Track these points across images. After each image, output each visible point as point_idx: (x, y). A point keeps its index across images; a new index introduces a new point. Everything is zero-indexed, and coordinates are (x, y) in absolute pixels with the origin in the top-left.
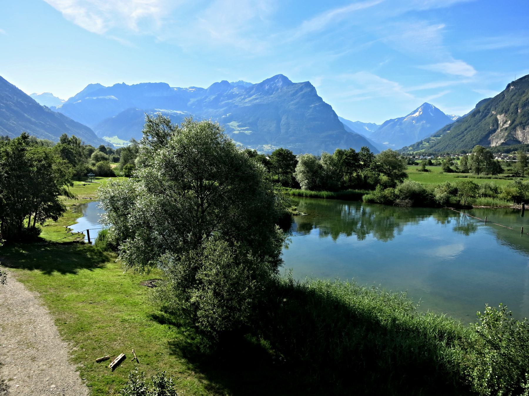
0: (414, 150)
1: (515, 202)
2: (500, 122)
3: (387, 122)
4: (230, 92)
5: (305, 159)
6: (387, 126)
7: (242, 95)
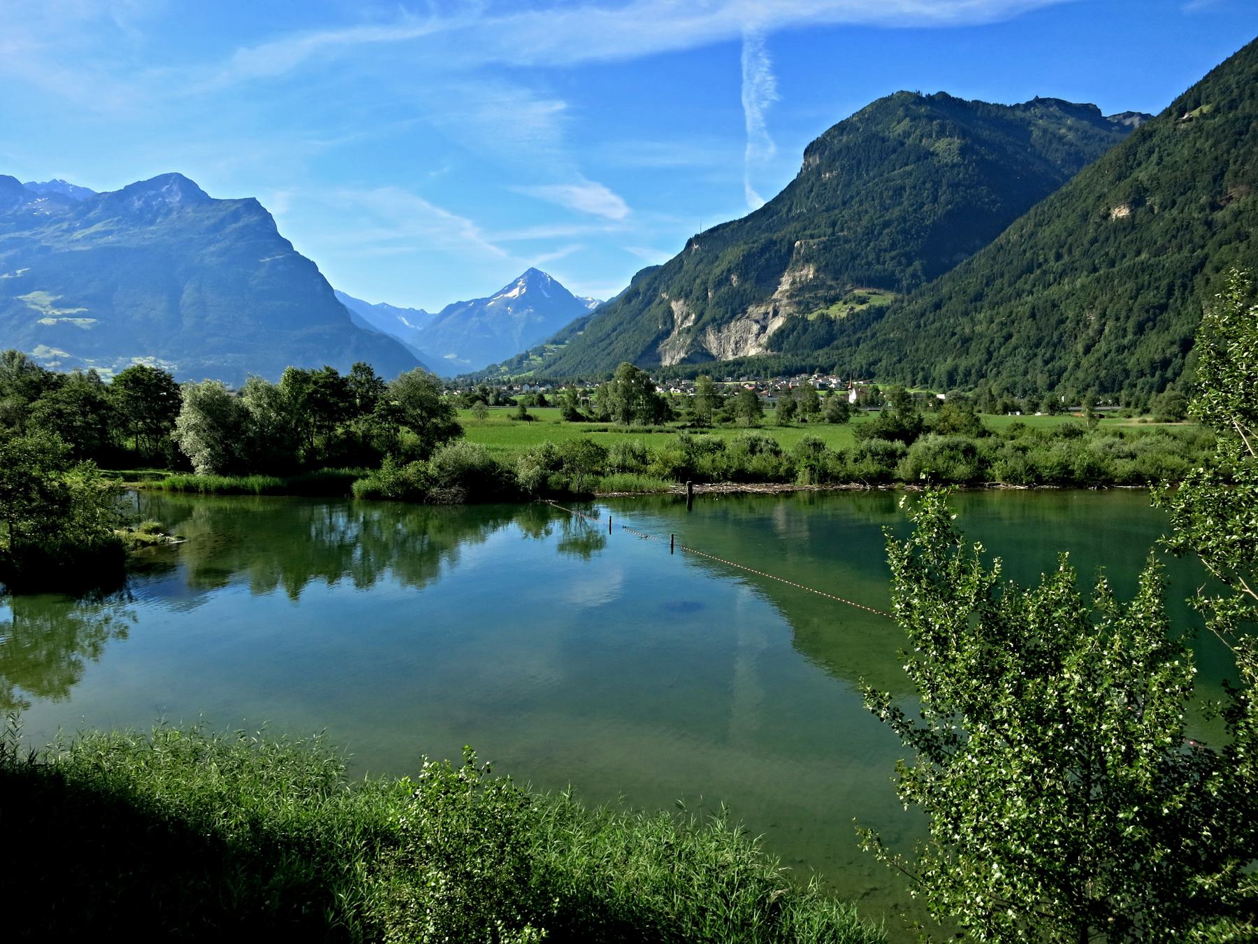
0: (511, 372)
1: (677, 480)
2: (677, 316)
3: (450, 309)
4: (24, 208)
5: (202, 393)
6: (451, 317)
7: (62, 220)
